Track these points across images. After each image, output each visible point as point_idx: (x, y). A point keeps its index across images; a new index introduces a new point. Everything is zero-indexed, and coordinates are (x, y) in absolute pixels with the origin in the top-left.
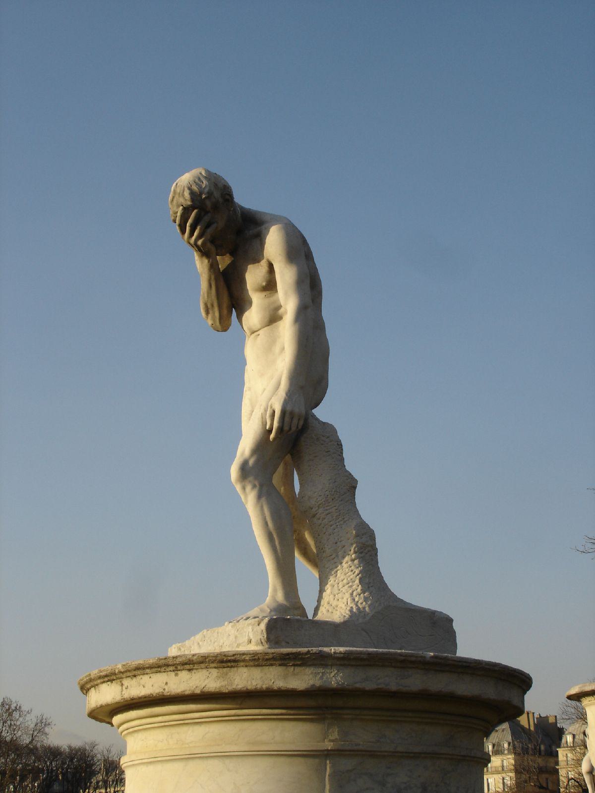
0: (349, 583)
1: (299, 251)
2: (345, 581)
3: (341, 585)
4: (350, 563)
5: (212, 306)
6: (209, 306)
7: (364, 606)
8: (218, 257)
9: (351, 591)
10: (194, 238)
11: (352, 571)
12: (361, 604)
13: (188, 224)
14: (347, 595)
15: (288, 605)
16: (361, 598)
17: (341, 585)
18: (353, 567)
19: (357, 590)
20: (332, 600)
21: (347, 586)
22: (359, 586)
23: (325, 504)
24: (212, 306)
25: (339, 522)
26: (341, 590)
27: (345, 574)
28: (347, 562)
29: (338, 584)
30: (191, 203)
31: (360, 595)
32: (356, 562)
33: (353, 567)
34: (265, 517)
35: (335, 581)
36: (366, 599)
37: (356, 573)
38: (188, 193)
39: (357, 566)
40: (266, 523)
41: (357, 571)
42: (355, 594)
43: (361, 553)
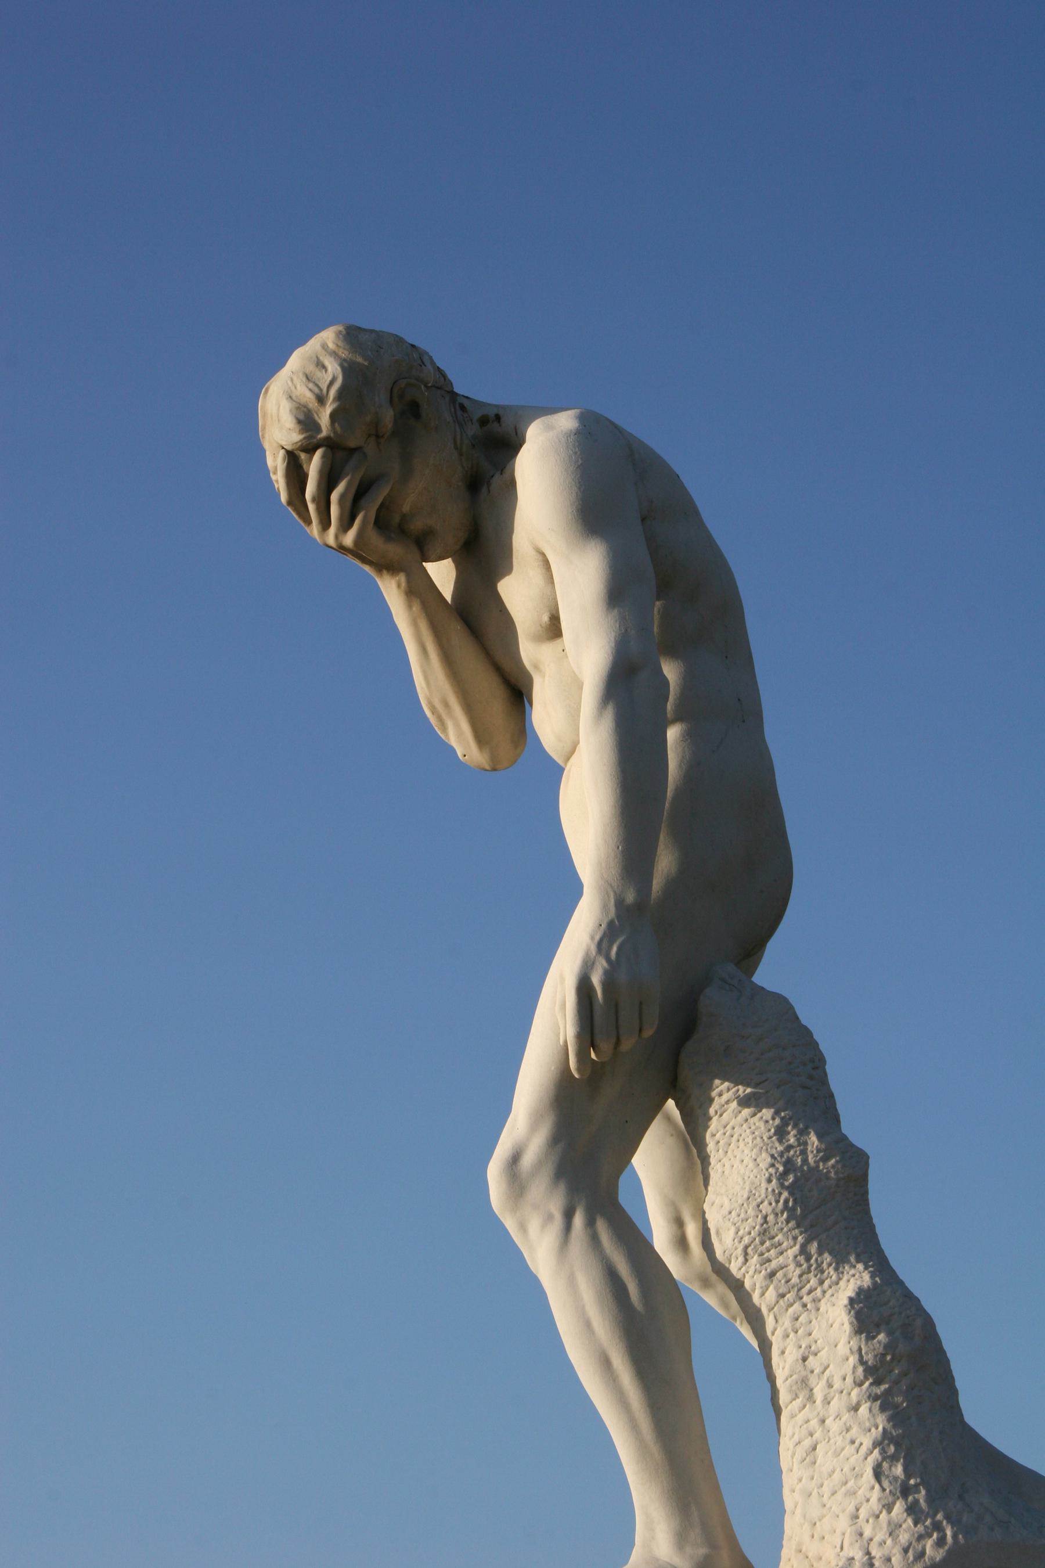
0: (846, 1483)
1: (633, 505)
2: (837, 1476)
3: (826, 1490)
4: (846, 1417)
5: (446, 705)
6: (439, 707)
7: (886, 1553)
8: (431, 567)
9: (851, 1508)
10: (332, 530)
11: (853, 1442)
12: (880, 1544)
13: (308, 496)
14: (843, 1523)
15: (891, 1412)
16: (881, 1528)
17: (826, 1490)
18: (855, 1431)
19: (868, 1500)
20: (806, 1538)
21: (843, 1489)
22: (873, 1488)
23: (762, 1243)
24: (446, 705)
25: (809, 1292)
26: (828, 1506)
27: (837, 1454)
28: (838, 1416)
29: (822, 1486)
30: (301, 437)
31: (878, 1517)
32: (864, 1410)
33: (855, 1431)
34: (583, 1307)
35: (812, 1478)
36: (893, 1530)
37: (864, 1450)
38: (288, 410)
39: (867, 1424)
40: (588, 1325)
41: (867, 1442)
42: (863, 1513)
43: (877, 1383)
